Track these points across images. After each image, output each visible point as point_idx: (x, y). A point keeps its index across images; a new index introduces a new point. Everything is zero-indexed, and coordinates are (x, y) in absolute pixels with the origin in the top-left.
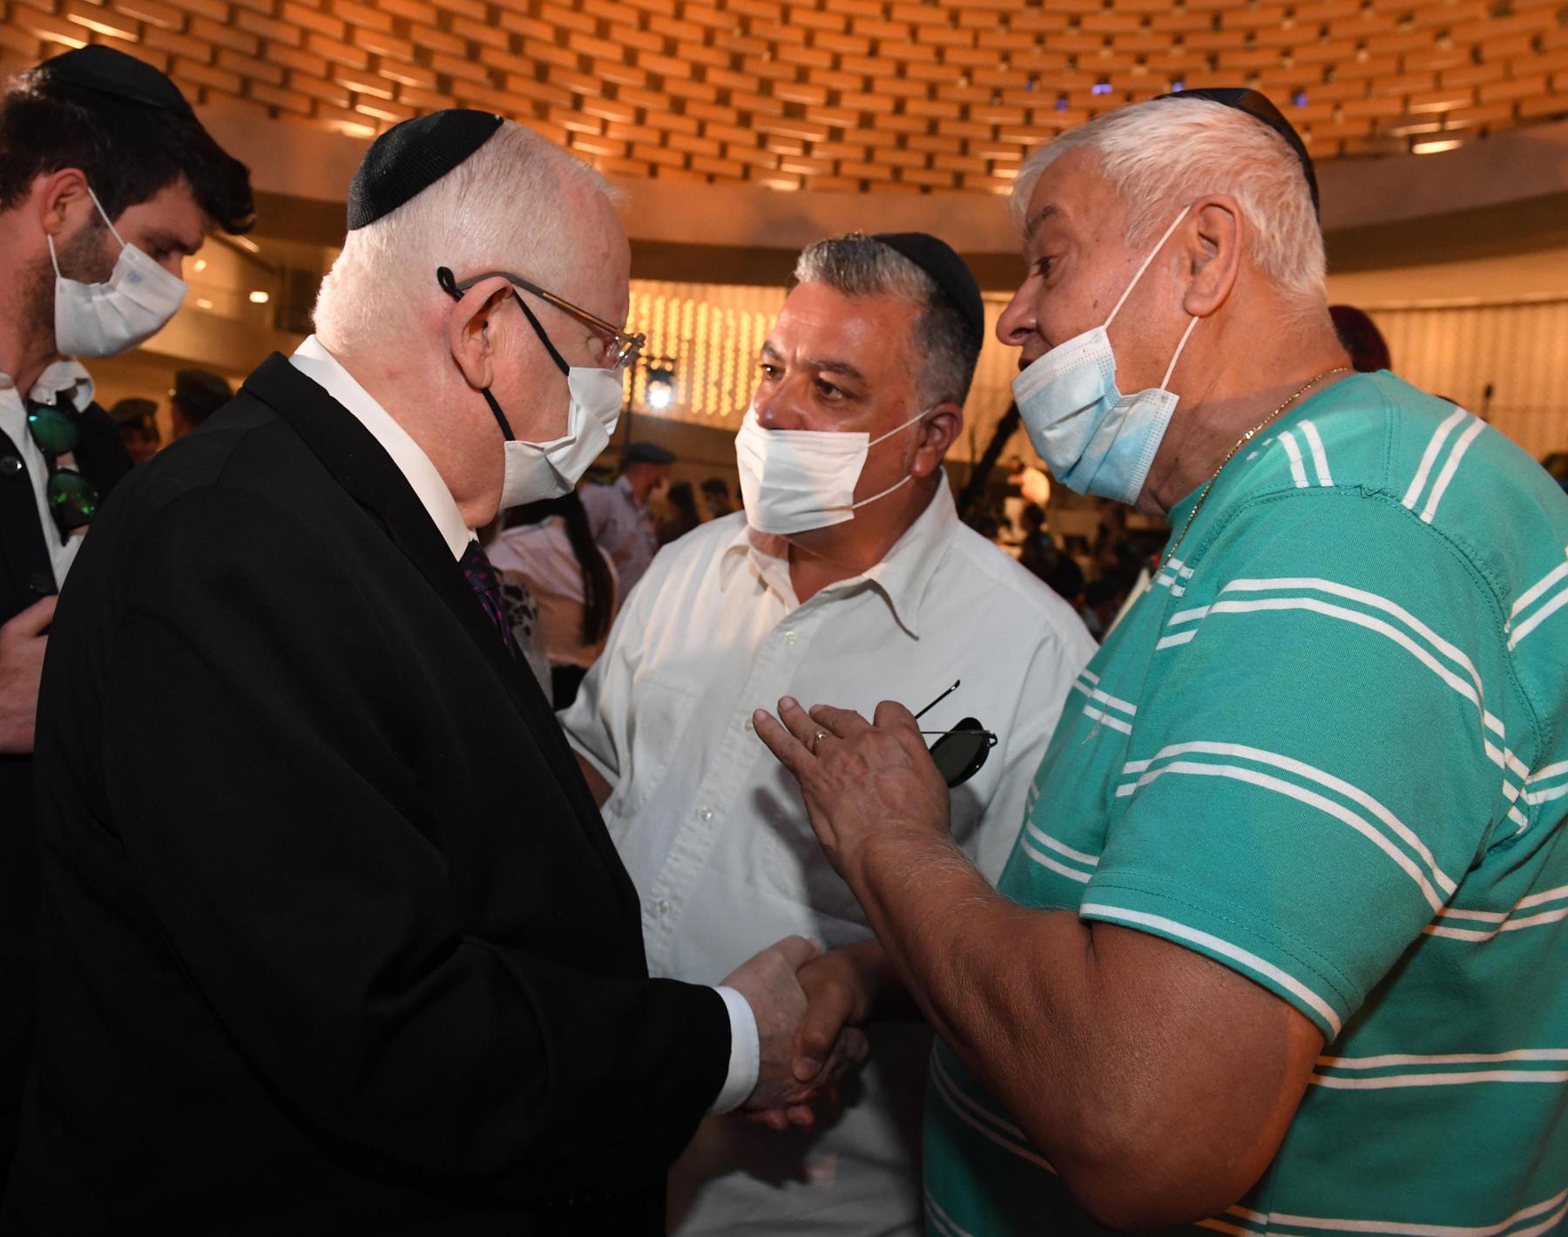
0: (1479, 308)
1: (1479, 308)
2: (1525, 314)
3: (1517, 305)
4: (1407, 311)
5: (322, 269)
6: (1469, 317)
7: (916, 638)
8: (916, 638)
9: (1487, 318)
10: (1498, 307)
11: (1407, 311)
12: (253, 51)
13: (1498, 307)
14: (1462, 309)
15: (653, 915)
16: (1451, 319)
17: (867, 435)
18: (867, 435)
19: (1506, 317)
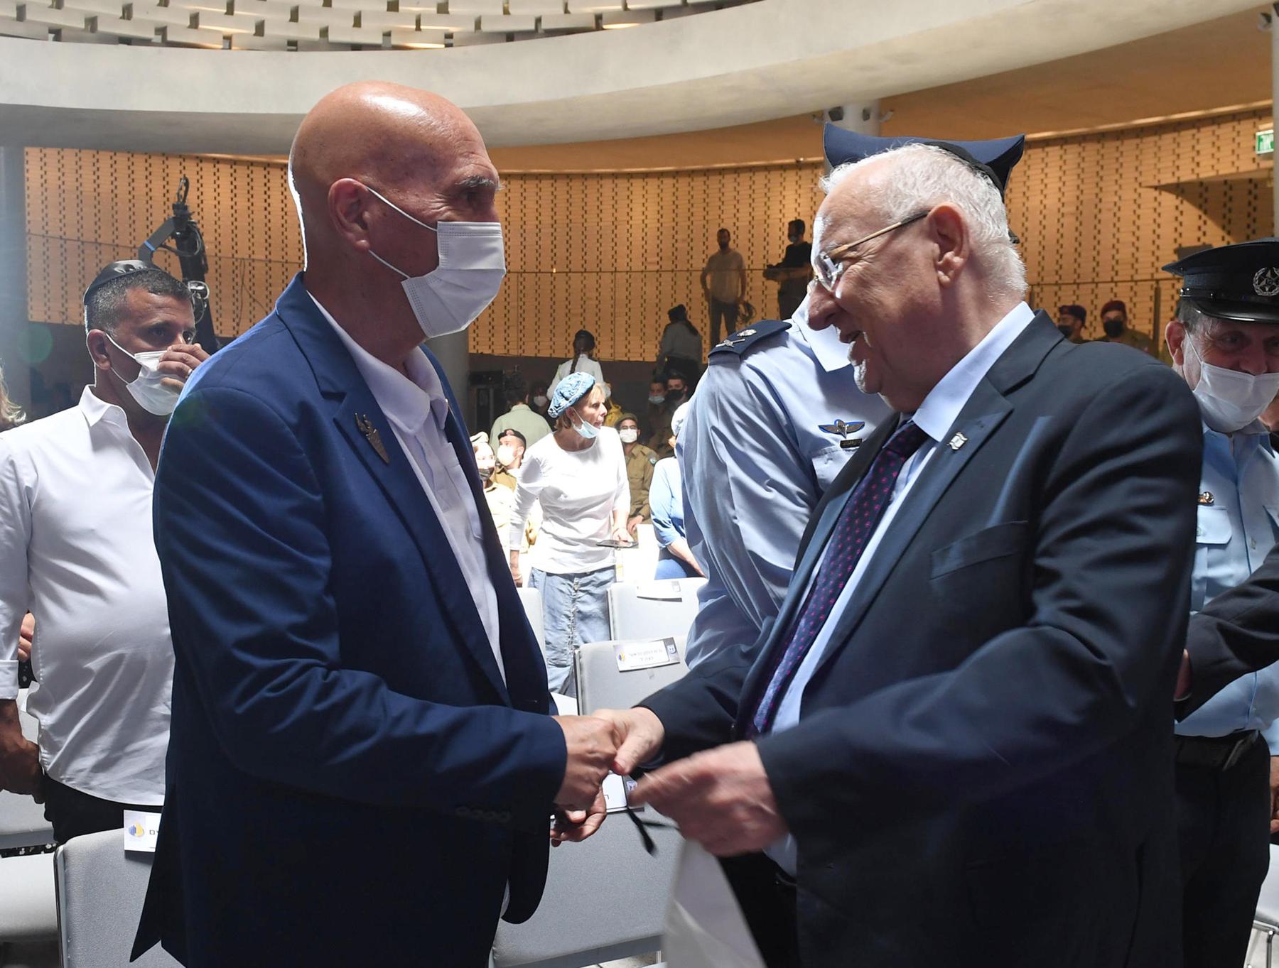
0: (675, 174)
1: (675, 174)
2: (714, 181)
3: (706, 173)
4: (767, 168)
5: (864, 157)
6: (668, 182)
7: (679, 600)
8: (679, 600)
9: (683, 183)
10: (691, 174)
11: (615, 176)
12: (14, 15)
13: (691, 174)
14: (661, 175)
15: (946, 196)
16: (653, 184)
17: (403, 283)
18: (403, 283)
19: (698, 182)
